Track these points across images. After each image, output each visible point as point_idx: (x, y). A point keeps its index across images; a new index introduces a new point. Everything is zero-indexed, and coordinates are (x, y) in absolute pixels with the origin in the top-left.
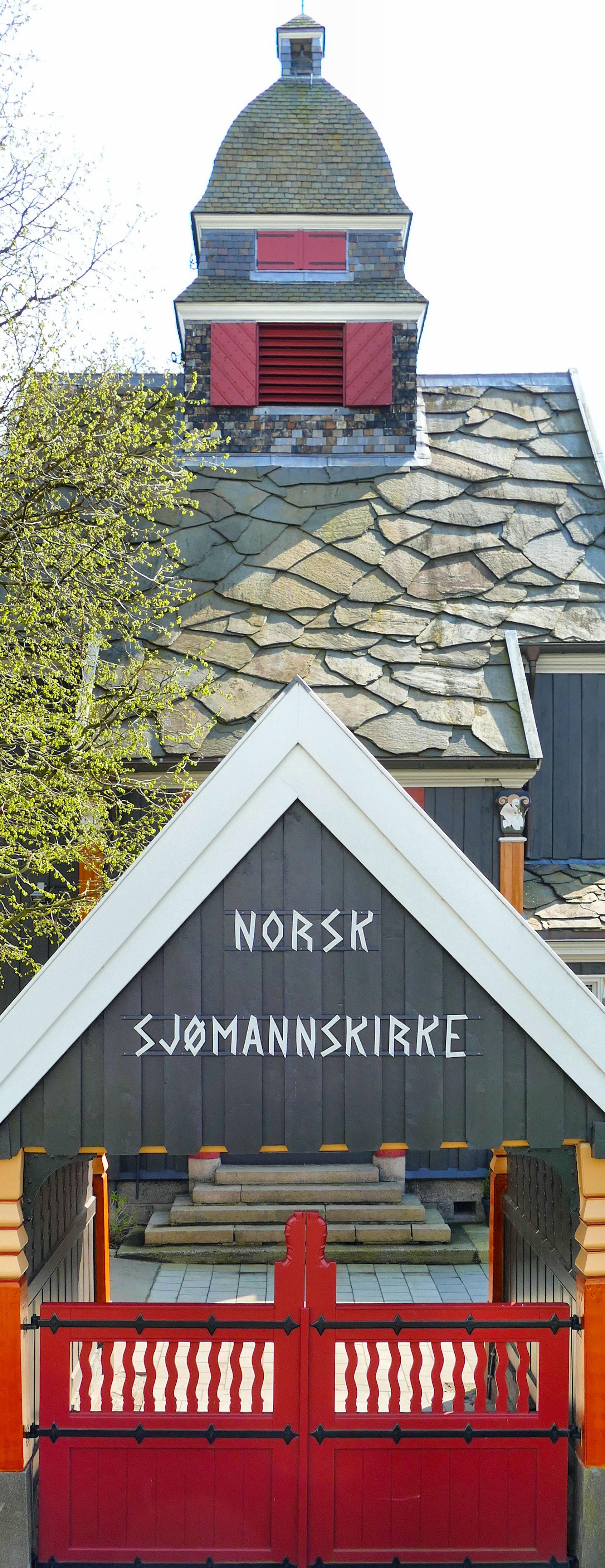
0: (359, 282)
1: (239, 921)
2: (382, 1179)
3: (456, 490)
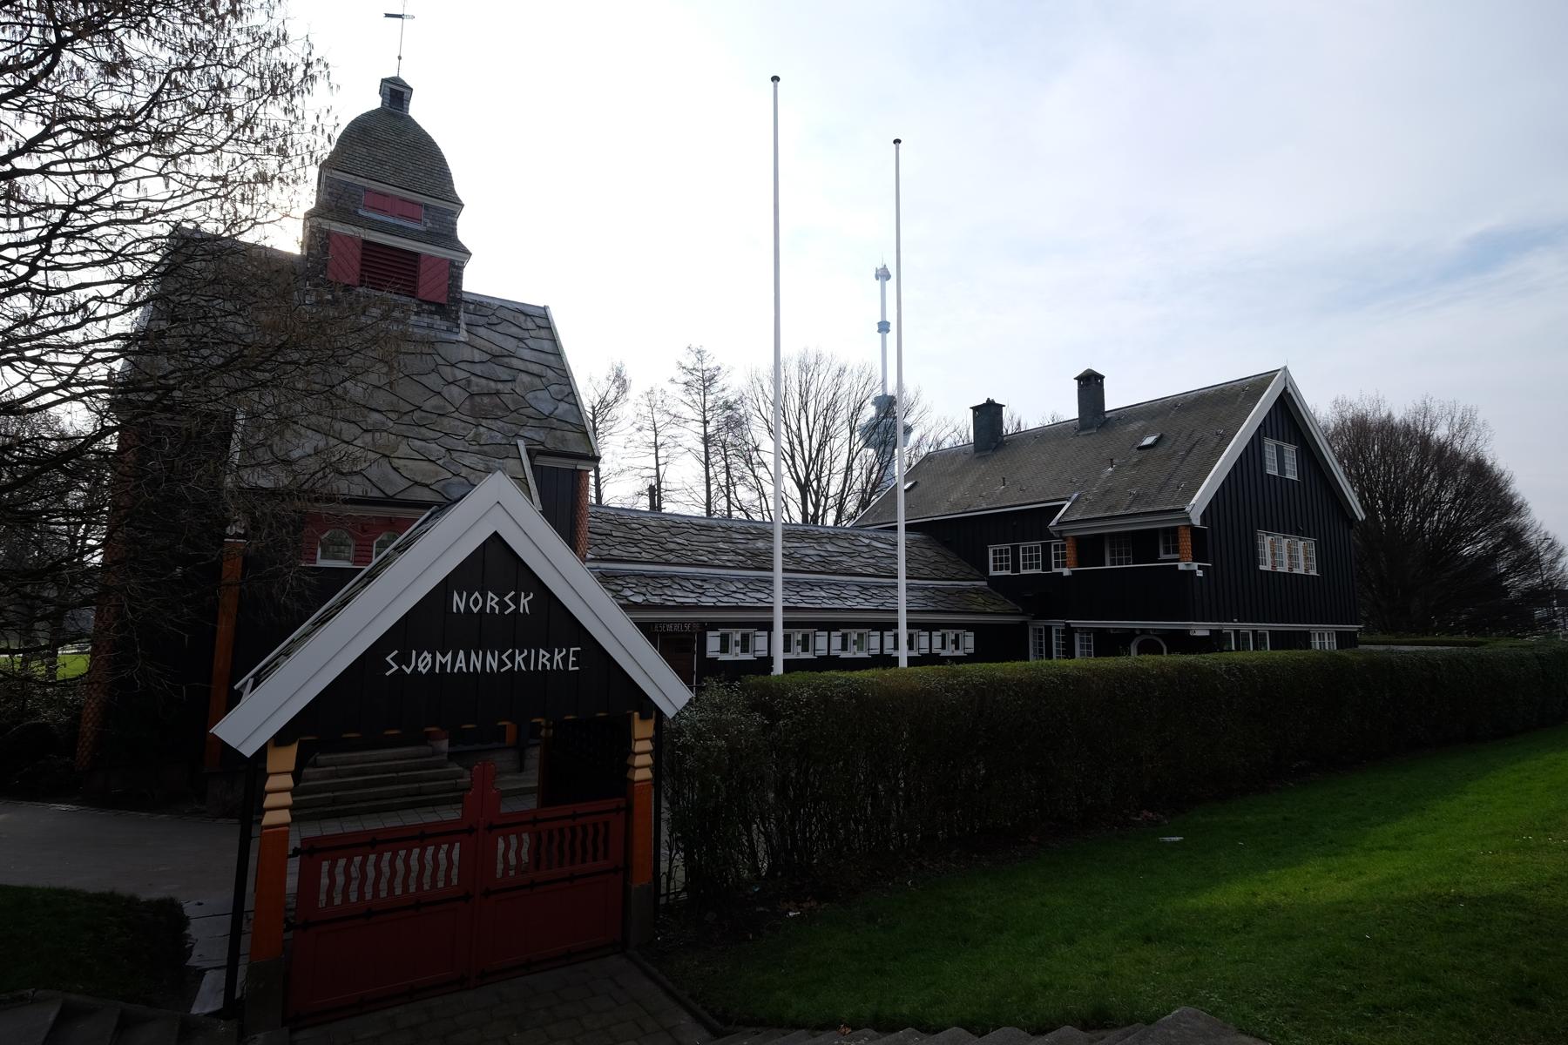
0: (428, 233)
1: (456, 597)
2: (434, 754)
3: (486, 357)
